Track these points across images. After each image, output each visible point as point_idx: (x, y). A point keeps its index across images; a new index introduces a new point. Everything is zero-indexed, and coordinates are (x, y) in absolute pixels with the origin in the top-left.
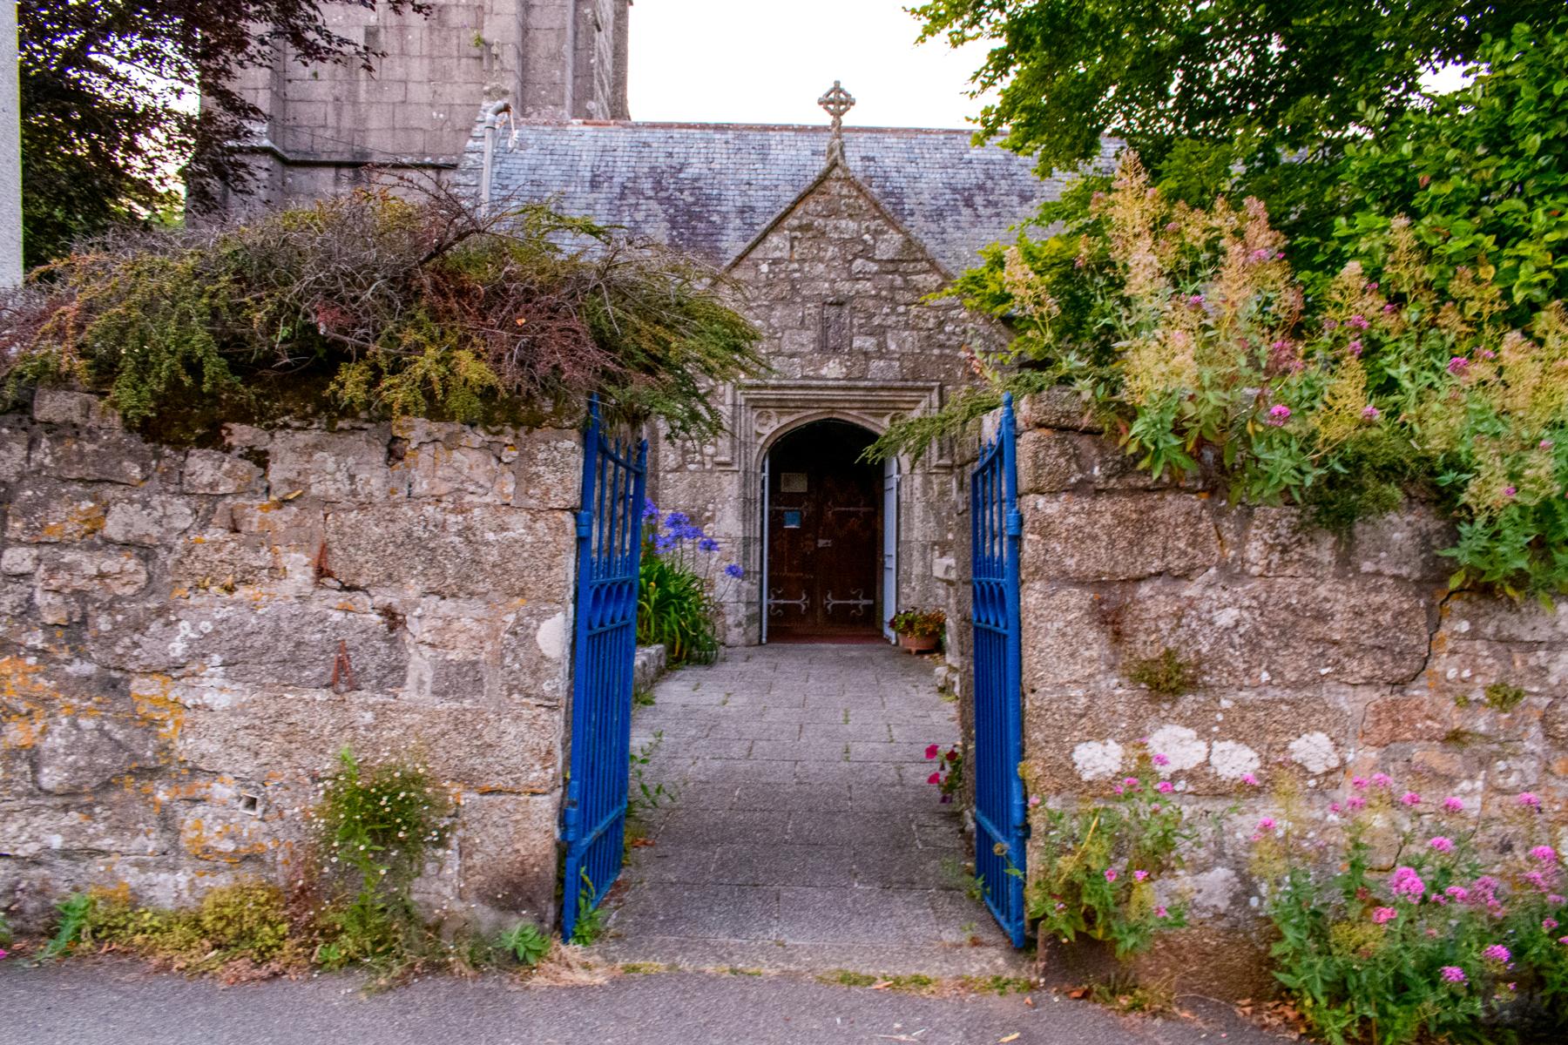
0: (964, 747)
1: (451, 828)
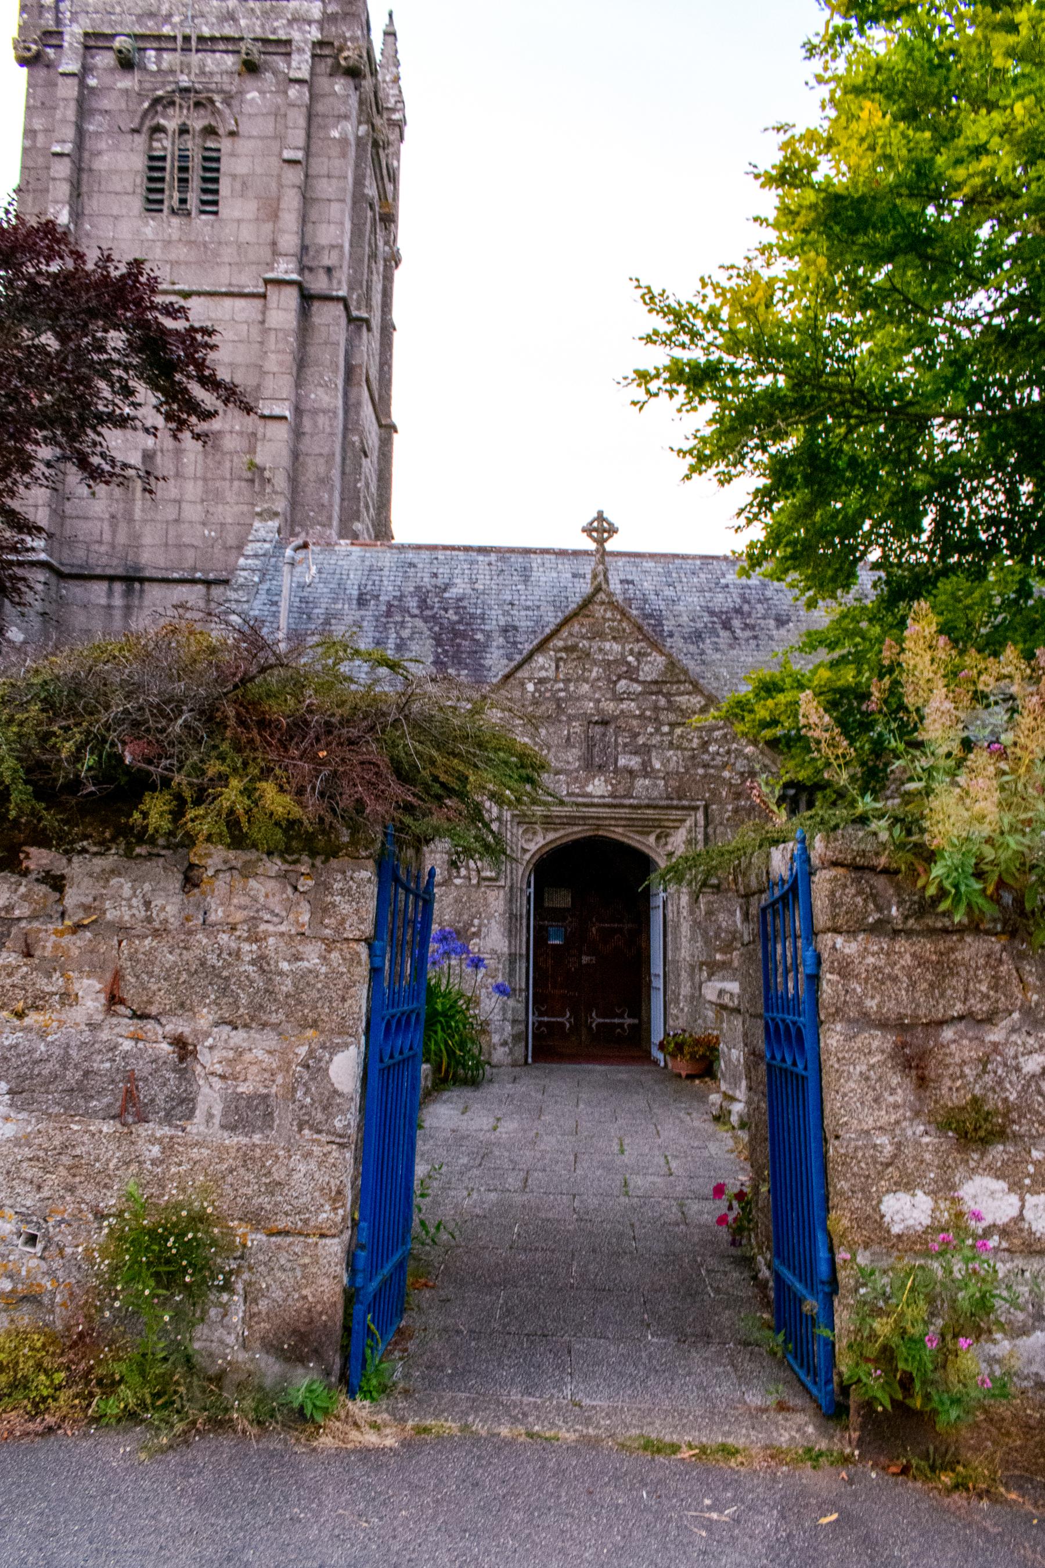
0: (756, 1189)
1: (238, 1272)
